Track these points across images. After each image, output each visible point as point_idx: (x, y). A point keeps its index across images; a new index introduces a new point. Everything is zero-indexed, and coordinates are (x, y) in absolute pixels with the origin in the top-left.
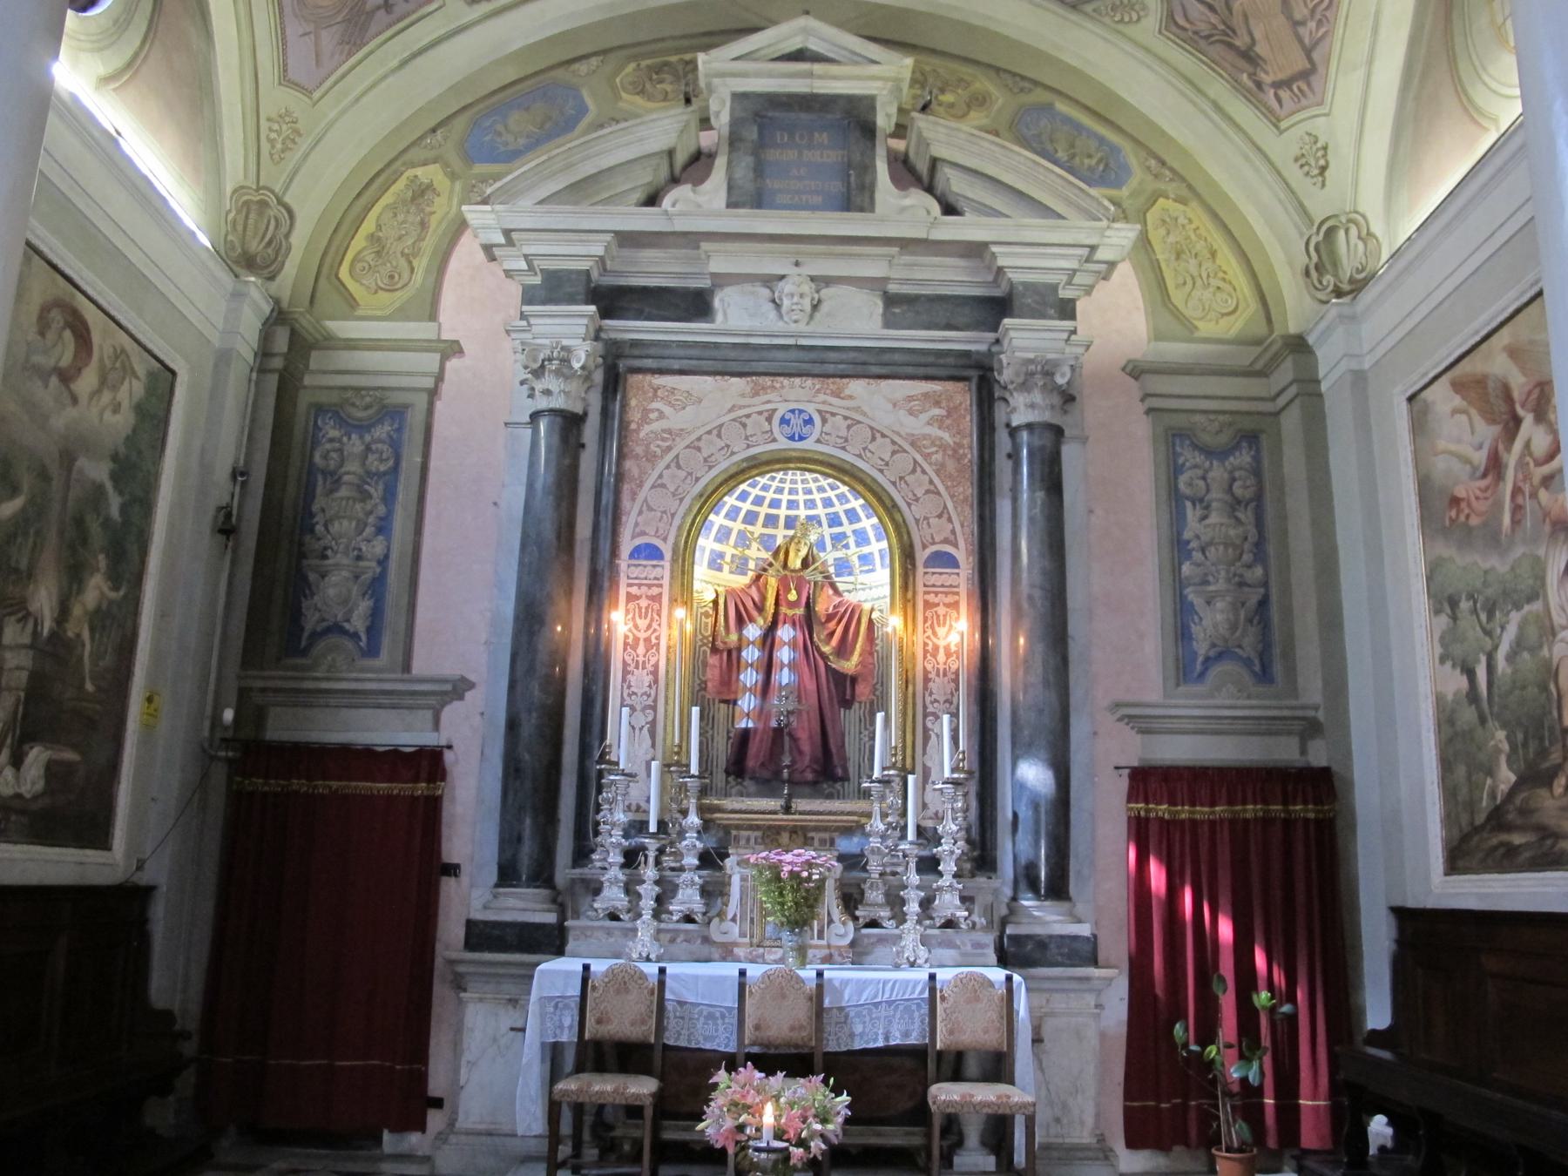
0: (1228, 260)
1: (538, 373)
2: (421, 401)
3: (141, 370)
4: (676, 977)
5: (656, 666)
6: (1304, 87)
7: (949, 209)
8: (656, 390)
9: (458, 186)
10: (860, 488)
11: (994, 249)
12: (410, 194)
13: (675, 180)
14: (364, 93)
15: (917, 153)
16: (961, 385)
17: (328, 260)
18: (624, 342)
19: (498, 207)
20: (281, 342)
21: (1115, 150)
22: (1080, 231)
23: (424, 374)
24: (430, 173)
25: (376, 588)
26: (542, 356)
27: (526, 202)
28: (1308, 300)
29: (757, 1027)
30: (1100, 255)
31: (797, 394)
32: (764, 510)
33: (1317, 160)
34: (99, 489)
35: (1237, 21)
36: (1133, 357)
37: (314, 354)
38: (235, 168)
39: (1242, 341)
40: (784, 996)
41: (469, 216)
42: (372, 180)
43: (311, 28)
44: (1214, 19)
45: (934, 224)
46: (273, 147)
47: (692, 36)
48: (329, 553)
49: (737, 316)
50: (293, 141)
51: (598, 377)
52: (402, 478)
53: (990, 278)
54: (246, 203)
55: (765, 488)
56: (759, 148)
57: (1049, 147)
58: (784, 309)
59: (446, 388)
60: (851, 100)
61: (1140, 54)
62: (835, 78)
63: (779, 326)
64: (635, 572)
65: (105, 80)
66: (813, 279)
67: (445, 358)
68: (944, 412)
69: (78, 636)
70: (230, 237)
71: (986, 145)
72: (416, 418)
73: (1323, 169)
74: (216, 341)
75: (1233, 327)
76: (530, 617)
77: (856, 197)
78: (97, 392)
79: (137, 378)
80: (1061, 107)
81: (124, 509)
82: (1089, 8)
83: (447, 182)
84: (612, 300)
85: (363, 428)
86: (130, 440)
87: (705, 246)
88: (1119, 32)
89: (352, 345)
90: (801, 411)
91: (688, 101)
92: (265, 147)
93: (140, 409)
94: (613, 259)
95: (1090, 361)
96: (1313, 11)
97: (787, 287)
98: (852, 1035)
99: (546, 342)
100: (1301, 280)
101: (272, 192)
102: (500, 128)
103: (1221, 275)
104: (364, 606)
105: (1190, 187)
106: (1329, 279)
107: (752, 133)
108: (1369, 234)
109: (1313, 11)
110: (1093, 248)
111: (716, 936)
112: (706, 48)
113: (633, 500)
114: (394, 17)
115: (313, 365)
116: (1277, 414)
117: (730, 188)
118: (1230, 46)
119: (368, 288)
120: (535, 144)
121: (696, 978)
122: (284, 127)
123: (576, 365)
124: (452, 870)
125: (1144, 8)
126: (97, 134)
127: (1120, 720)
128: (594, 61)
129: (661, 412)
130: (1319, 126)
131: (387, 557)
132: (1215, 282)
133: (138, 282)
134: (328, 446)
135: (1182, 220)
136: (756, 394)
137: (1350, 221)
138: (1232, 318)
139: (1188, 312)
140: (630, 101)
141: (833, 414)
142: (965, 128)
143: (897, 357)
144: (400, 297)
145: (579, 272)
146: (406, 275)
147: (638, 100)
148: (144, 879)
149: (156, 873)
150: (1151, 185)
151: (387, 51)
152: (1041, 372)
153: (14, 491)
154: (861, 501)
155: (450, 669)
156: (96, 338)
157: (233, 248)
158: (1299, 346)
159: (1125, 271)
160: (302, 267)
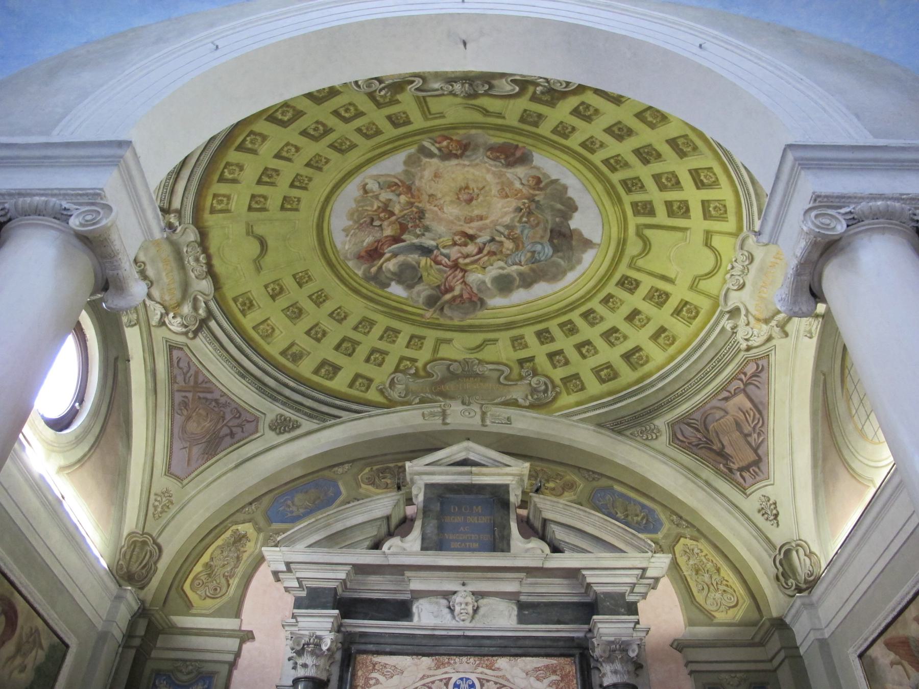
0: (727, 573)
1: (300, 653)
3: (45, 643)
6: (757, 470)
7: (555, 549)
8: (374, 665)
9: (261, 536)
11: (584, 572)
13: (390, 535)
15: (534, 516)
16: (569, 659)
17: (178, 579)
18: (355, 633)
19: (283, 549)
20: (141, 630)
21: (651, 511)
22: (635, 559)
23: (229, 652)
24: (246, 528)
26: (303, 642)
27: (301, 546)
28: (781, 595)
30: (649, 573)
33: (772, 511)
35: (712, 435)
36: (677, 637)
38: (131, 522)
39: (743, 624)
41: (266, 554)
43: (187, 445)
45: (546, 558)
46: (156, 510)
47: (403, 453)
49: (427, 617)
50: (168, 507)
51: (338, 656)
53: (583, 591)
54: (135, 542)
56: (441, 515)
57: (613, 512)
58: (456, 612)
59: (242, 662)
62: (484, 475)
63: (453, 624)
65: (62, 469)
66: (473, 593)
68: (559, 678)
70: (121, 562)
71: (575, 510)
73: (776, 516)
74: (100, 627)
75: (737, 614)
77: (500, 544)
79: (42, 648)
80: (617, 488)
82: (628, 433)
83: (255, 533)
84: (348, 606)
87: (408, 574)
90: (467, 679)
91: (399, 488)
93: (39, 670)
94: (351, 581)
95: (650, 641)
96: (754, 428)
97: (458, 599)
99: (307, 633)
100: (775, 584)
101: (151, 536)
102: (289, 502)
103: (724, 582)
105: (698, 530)
106: (791, 581)
107: (437, 507)
108: (811, 552)
109: (754, 428)
110: (644, 570)
112: (410, 459)
114: (235, 440)
115: (159, 644)
116: (775, 670)
117: (423, 539)
118: (711, 449)
119: (200, 596)
122: (164, 499)
123: (324, 648)
125: (659, 431)
126: (50, 498)
128: (346, 466)
129: (377, 680)
130: (769, 491)
132: (722, 588)
133: (56, 588)
135: (696, 551)
136: (438, 668)
137: (798, 545)
138: (735, 609)
139: (708, 607)
140: (365, 488)
141: (488, 681)
142: (561, 501)
143: (527, 643)
145: (330, 589)
146: (224, 590)
147: (370, 487)
150: (676, 531)
152: (619, 649)
156: (20, 621)
157: (122, 568)
158: (780, 625)
159: (665, 583)
160: (162, 582)
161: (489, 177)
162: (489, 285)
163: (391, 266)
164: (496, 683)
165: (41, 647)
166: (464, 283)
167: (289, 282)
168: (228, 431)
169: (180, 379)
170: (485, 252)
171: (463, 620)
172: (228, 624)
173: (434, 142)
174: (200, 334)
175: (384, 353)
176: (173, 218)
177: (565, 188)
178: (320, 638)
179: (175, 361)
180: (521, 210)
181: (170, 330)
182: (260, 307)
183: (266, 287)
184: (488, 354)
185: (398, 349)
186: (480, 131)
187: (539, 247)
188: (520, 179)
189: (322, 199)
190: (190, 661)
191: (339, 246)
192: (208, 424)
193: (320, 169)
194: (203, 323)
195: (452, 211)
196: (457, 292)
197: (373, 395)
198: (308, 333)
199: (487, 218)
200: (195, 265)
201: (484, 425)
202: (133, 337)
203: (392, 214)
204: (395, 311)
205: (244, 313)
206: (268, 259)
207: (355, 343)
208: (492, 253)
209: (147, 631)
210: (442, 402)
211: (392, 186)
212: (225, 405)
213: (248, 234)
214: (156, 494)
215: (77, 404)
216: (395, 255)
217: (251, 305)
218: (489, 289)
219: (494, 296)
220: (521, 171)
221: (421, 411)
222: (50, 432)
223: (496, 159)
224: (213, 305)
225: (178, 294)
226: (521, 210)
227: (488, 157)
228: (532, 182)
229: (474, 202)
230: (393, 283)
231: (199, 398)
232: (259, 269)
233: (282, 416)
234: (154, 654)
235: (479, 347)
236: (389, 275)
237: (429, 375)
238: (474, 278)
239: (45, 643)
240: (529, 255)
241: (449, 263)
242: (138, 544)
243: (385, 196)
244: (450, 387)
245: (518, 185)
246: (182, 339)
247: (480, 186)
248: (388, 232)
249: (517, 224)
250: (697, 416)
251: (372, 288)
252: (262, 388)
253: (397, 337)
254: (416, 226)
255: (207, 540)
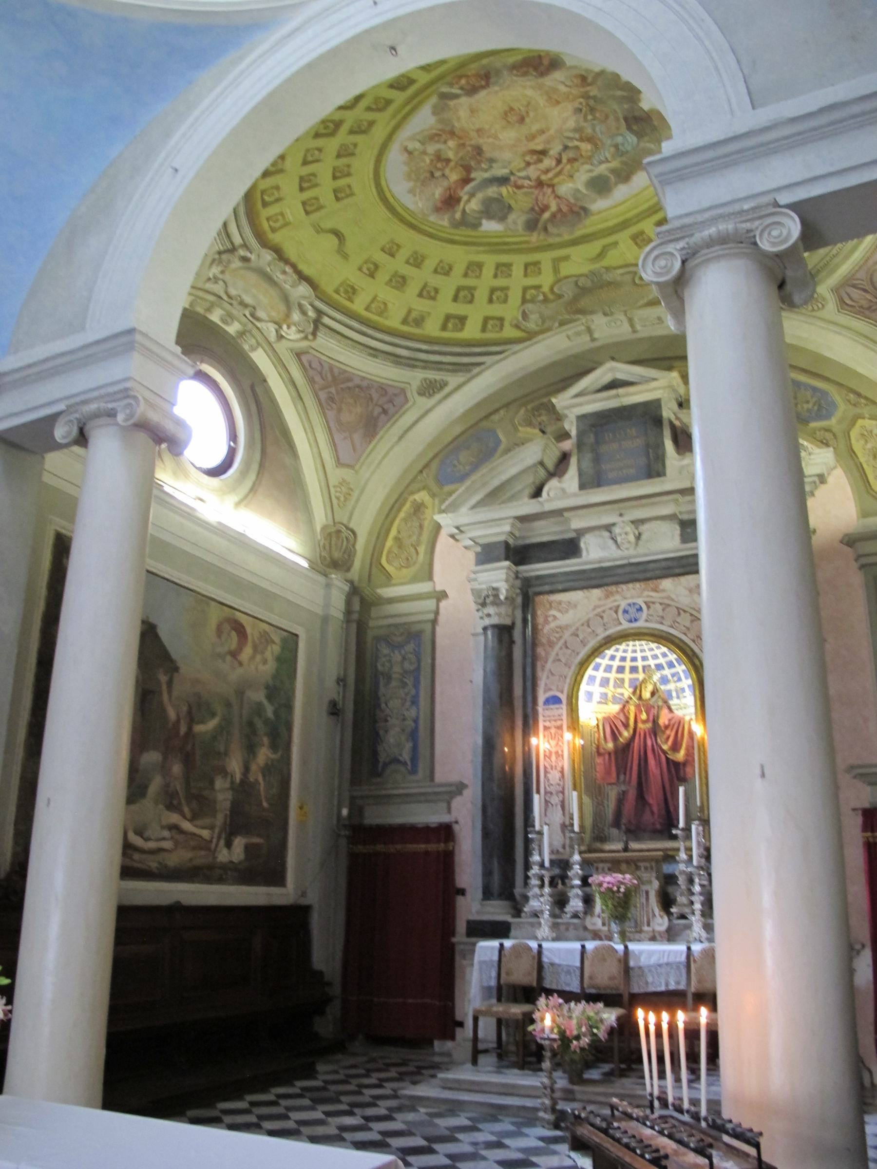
2: (429, 627)
3: (277, 639)
4: (550, 950)
5: (562, 768)
8: (550, 604)
9: (437, 501)
10: (672, 647)
12: (412, 510)
14: (383, 458)
20: (356, 607)
21: (824, 393)
25: (413, 735)
27: (464, 509)
29: (591, 978)
31: (632, 594)
32: (628, 664)
34: (260, 705)
37: (372, 608)
38: (320, 517)
40: (605, 960)
42: (392, 507)
44: (869, 297)
48: (389, 718)
49: (595, 552)
51: (519, 600)
52: (422, 673)
54: (330, 535)
55: (613, 658)
59: (442, 619)
60: (646, 404)
61: (831, 327)
64: (547, 713)
65: (238, 504)
66: (633, 522)
67: (439, 600)
69: (257, 780)
72: (427, 637)
76: (490, 746)
78: (252, 658)
81: (276, 713)
84: (519, 553)
85: (400, 646)
86: (276, 676)
87: (566, 514)
88: (814, 317)
89: (391, 601)
90: (634, 604)
91: (543, 432)
92: (335, 501)
93: (278, 659)
97: (617, 530)
98: (647, 983)
104: (409, 745)
107: (591, 439)
111: (590, 927)
113: (543, 670)
120: (475, 467)
121: (559, 950)
123: (502, 597)
124: (462, 892)
125: (824, 299)
127: (855, 777)
128: (502, 412)
131: (418, 717)
133: (267, 597)
134: (384, 659)
141: (653, 603)
144: (413, 570)
145: (499, 542)
148: (304, 902)
149: (312, 898)
151: (389, 435)
153: (213, 715)
154: (675, 656)
155: (454, 778)
156: (249, 630)
160: (363, 561)
161: (529, 92)
162: (584, 191)
163: (474, 205)
164: (661, 604)
165: (273, 642)
166: (557, 197)
167: (380, 257)
168: (380, 410)
169: (318, 379)
170: (564, 160)
171: (627, 549)
172: (423, 587)
173: (451, 85)
174: (319, 334)
175: (504, 289)
176: (242, 252)
177: (617, 76)
178: (496, 589)
179: (307, 365)
180: (581, 110)
181: (289, 340)
182: (362, 289)
183: (360, 269)
184: (613, 258)
185: (517, 281)
186: (492, 58)
187: (619, 139)
188: (563, 83)
189: (371, 176)
190: (400, 624)
191: (411, 207)
192: (359, 411)
193: (353, 154)
194: (317, 323)
195: (508, 136)
196: (554, 208)
197: (509, 332)
198: (420, 295)
199: (548, 130)
200: (285, 278)
201: (634, 331)
202: (260, 359)
203: (448, 161)
204: (496, 246)
205: (350, 300)
206: (351, 245)
207: (471, 290)
208: (571, 161)
209: (361, 605)
210: (583, 319)
211: (433, 137)
212: (368, 388)
213: (318, 232)
214: (334, 487)
215: (232, 444)
216: (472, 195)
217: (354, 291)
218: (585, 195)
219: (595, 201)
220: (558, 75)
221: (564, 334)
222: (214, 482)
223: (525, 74)
224: (319, 304)
225: (282, 307)
226: (581, 110)
227: (516, 75)
228: (578, 81)
229: (527, 120)
230: (484, 222)
231: (342, 389)
232: (345, 256)
233: (425, 379)
234: (371, 624)
235: (601, 255)
236: (477, 215)
237: (560, 296)
238: (565, 188)
239: (277, 639)
240: (612, 149)
241: (532, 184)
242: (334, 536)
243: (431, 149)
244: (583, 303)
245: (563, 89)
246: (304, 344)
247: (525, 103)
248: (454, 177)
249: (585, 124)
250: (862, 275)
251: (464, 233)
252: (397, 360)
253: (511, 270)
254: (479, 162)
255: (391, 516)
